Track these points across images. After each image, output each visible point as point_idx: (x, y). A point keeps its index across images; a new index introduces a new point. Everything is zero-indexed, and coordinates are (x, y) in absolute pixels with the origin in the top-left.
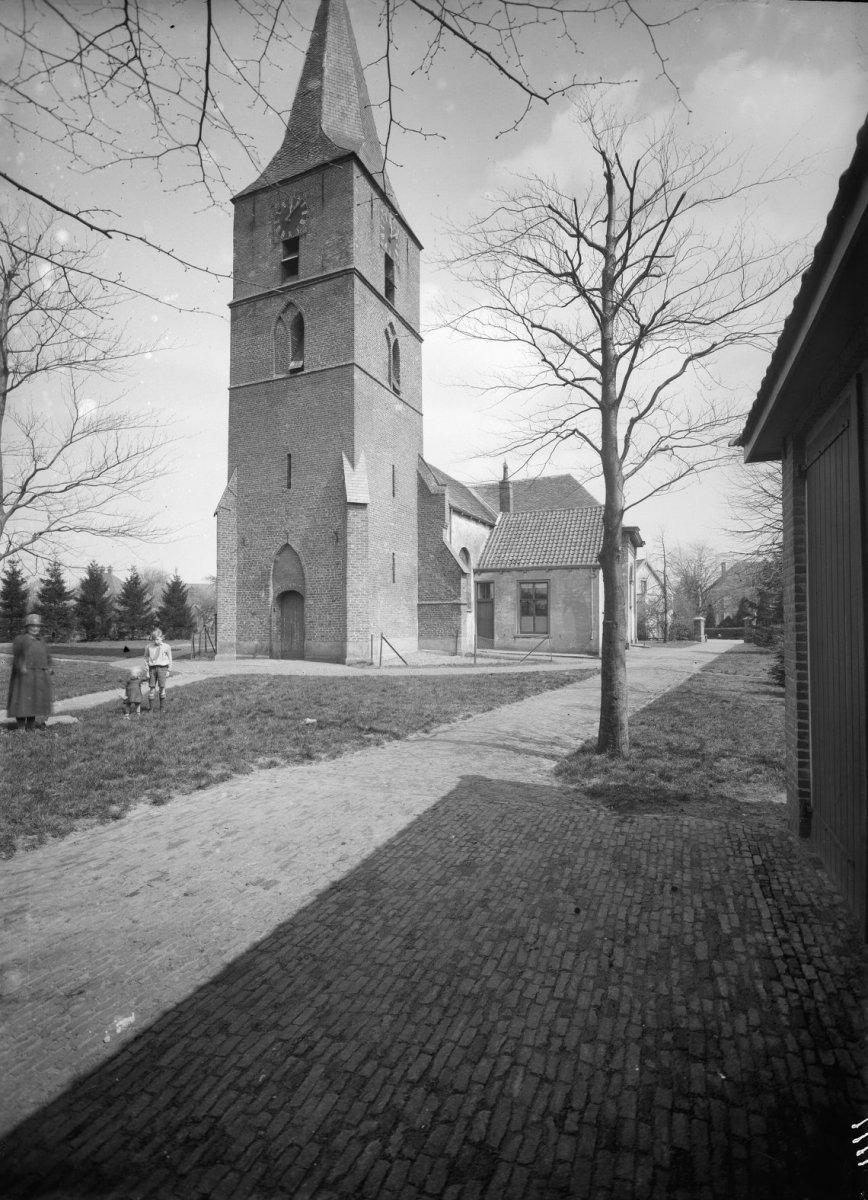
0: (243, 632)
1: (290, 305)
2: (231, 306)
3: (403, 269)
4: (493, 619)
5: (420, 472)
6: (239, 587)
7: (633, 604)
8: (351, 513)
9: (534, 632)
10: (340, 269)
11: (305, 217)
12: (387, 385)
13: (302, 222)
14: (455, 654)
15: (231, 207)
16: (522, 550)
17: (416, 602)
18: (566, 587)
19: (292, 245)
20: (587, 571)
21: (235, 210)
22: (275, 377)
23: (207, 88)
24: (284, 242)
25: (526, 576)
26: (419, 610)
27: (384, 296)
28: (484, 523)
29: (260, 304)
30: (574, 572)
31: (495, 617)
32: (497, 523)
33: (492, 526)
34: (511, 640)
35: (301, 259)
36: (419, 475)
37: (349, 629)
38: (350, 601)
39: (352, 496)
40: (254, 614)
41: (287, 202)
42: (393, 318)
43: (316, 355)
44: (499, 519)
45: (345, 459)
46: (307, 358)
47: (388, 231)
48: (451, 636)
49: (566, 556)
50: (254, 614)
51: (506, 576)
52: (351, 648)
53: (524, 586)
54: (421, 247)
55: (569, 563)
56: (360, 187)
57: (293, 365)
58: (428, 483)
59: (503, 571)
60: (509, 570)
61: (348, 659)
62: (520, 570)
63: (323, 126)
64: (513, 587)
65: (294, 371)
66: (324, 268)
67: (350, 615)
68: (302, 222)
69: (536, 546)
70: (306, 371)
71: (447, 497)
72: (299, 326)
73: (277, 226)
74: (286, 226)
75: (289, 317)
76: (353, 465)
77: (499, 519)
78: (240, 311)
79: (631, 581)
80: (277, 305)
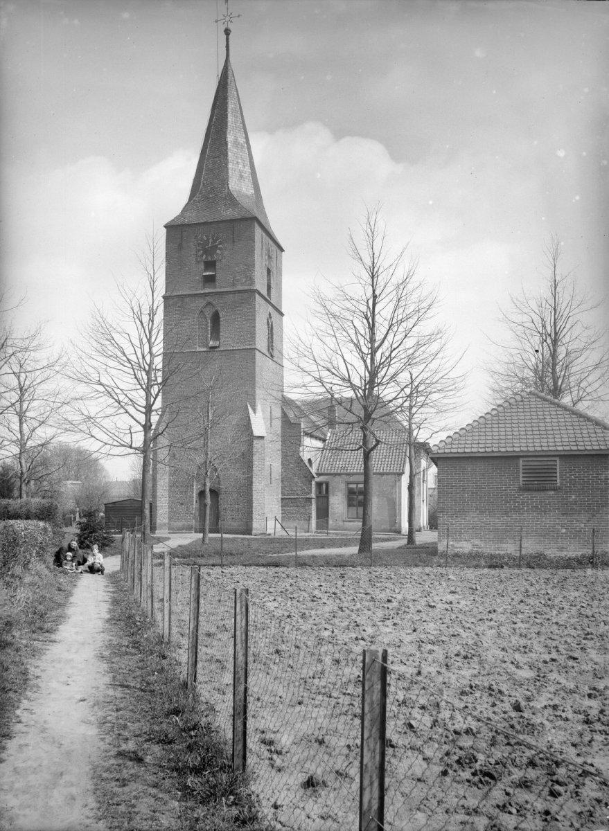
0: (173, 515)
1: (209, 304)
2: (164, 297)
3: (275, 272)
4: (328, 509)
5: (284, 407)
6: (170, 486)
7: (425, 498)
8: (255, 442)
9: (357, 518)
10: (246, 288)
11: (220, 249)
12: (267, 354)
13: (218, 251)
14: (308, 532)
15: (165, 230)
16: (348, 460)
17: (280, 497)
18: (379, 487)
19: (210, 265)
20: (394, 476)
21: (167, 233)
22: (198, 349)
23: (344, 360)
24: (204, 262)
25: (352, 479)
26: (282, 502)
27: (266, 297)
28: (320, 439)
29: (187, 300)
30: (385, 477)
31: (330, 507)
32: (328, 438)
33: (324, 441)
34: (341, 523)
35: (218, 275)
36: (282, 409)
37: (254, 513)
38: (254, 496)
39: (256, 432)
40: (182, 504)
41: (207, 236)
42: (270, 309)
43: (228, 338)
44: (329, 434)
45: (249, 408)
46: (222, 340)
47: (268, 250)
48: (305, 519)
49: (379, 466)
50: (182, 504)
51: (337, 479)
52: (255, 525)
53: (351, 486)
54: (282, 250)
55: (381, 471)
56: (258, 232)
57: (211, 343)
58: (289, 415)
59: (335, 475)
60: (339, 474)
61: (254, 532)
62: (347, 474)
63: (230, 186)
64: (343, 486)
65: (213, 348)
66: (234, 285)
67: (254, 505)
68: (218, 251)
69: (358, 457)
70: (222, 349)
71: (302, 426)
72: (216, 319)
73: (199, 250)
74: (206, 252)
75: (209, 313)
76: (254, 411)
77: (329, 434)
78: (171, 302)
79: (424, 481)
80: (201, 303)
